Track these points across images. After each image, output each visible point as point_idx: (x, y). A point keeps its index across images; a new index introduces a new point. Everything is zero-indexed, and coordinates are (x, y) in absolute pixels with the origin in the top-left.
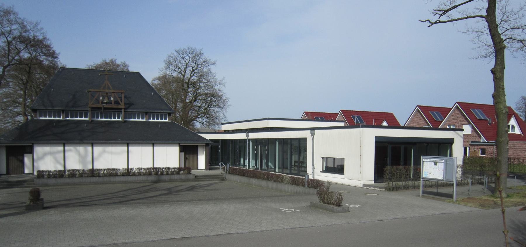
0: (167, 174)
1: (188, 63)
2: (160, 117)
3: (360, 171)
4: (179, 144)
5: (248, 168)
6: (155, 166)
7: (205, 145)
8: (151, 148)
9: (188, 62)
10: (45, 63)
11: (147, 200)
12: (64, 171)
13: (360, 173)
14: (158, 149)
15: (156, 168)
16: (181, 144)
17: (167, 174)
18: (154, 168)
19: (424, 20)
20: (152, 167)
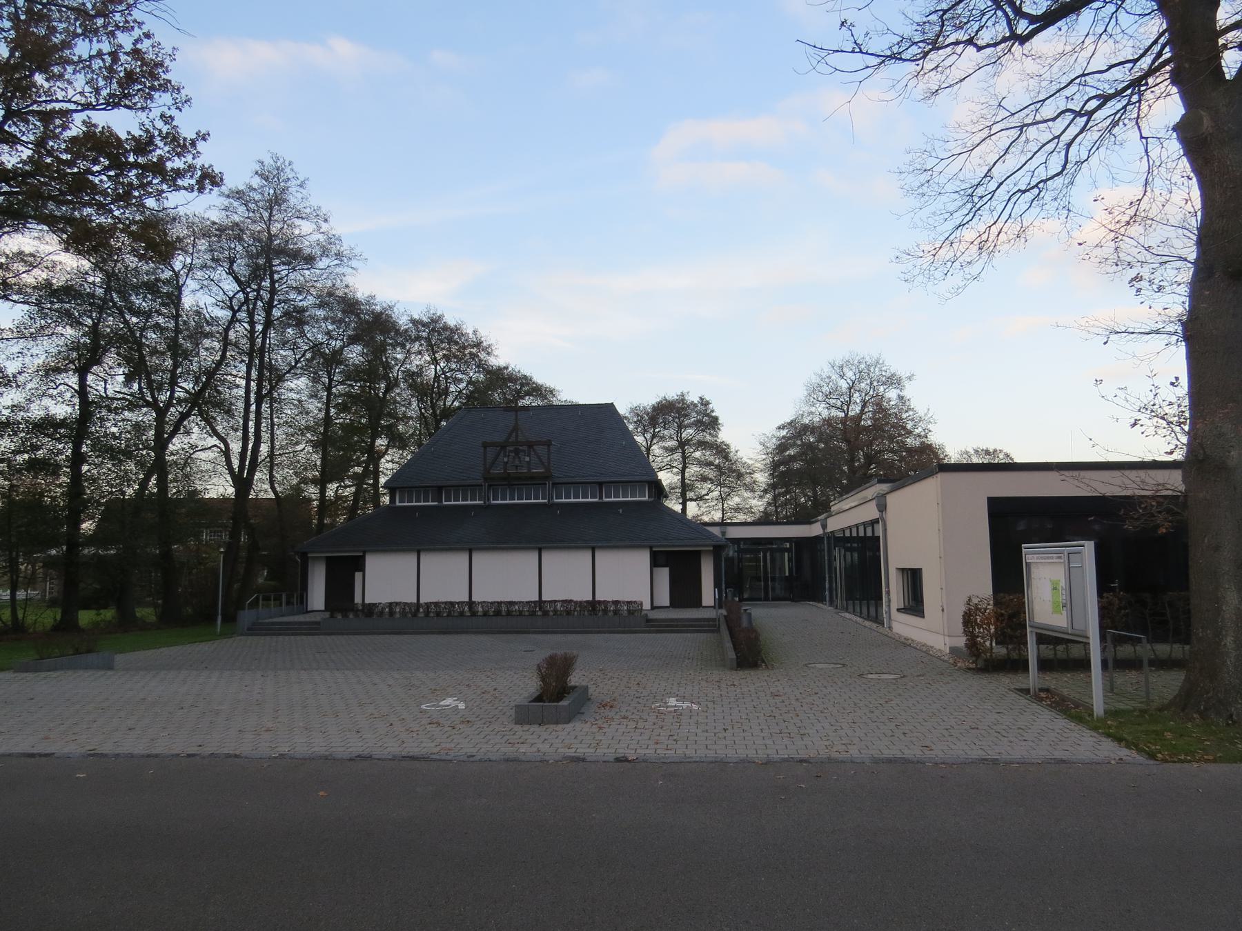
0: (509, 613)
1: (853, 384)
2: (399, 496)
3: (942, 606)
4: (651, 548)
5: (676, 602)
6: (598, 598)
7: (712, 549)
8: (534, 556)
9: (853, 383)
10: (84, 449)
11: (1019, 695)
12: (418, 604)
13: (943, 610)
14: (426, 559)
15: (600, 602)
16: (654, 549)
17: (509, 613)
18: (540, 602)
19: (1060, 169)
20: (590, 598)
